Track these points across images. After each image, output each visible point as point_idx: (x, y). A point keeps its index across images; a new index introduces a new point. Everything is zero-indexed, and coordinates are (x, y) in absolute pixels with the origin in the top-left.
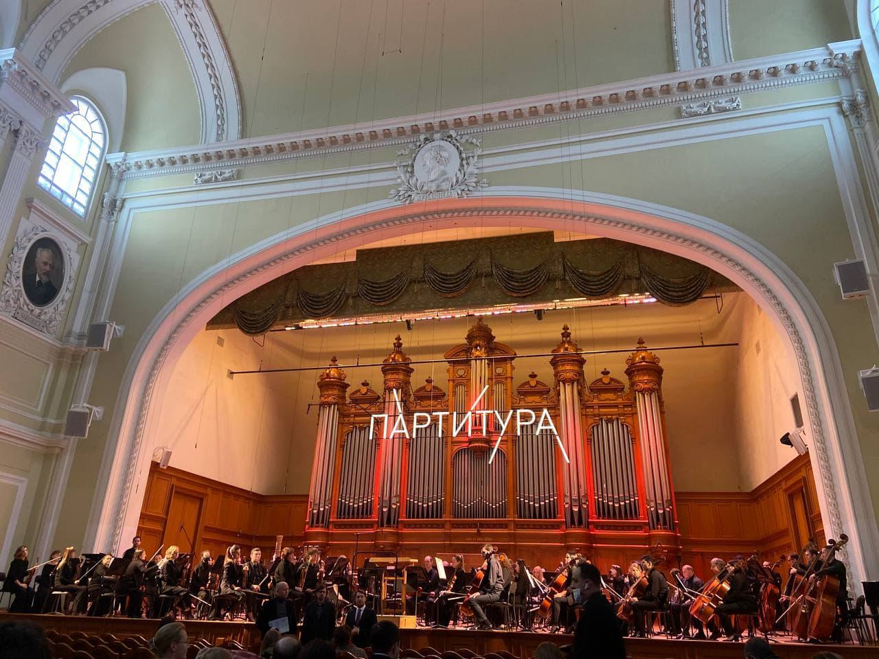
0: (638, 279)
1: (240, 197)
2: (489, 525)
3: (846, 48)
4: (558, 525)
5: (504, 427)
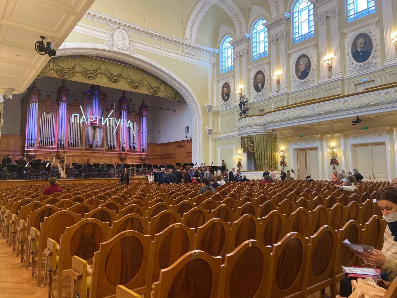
0: (164, 91)
1: (92, 34)
3: (216, 51)
4: (81, 149)
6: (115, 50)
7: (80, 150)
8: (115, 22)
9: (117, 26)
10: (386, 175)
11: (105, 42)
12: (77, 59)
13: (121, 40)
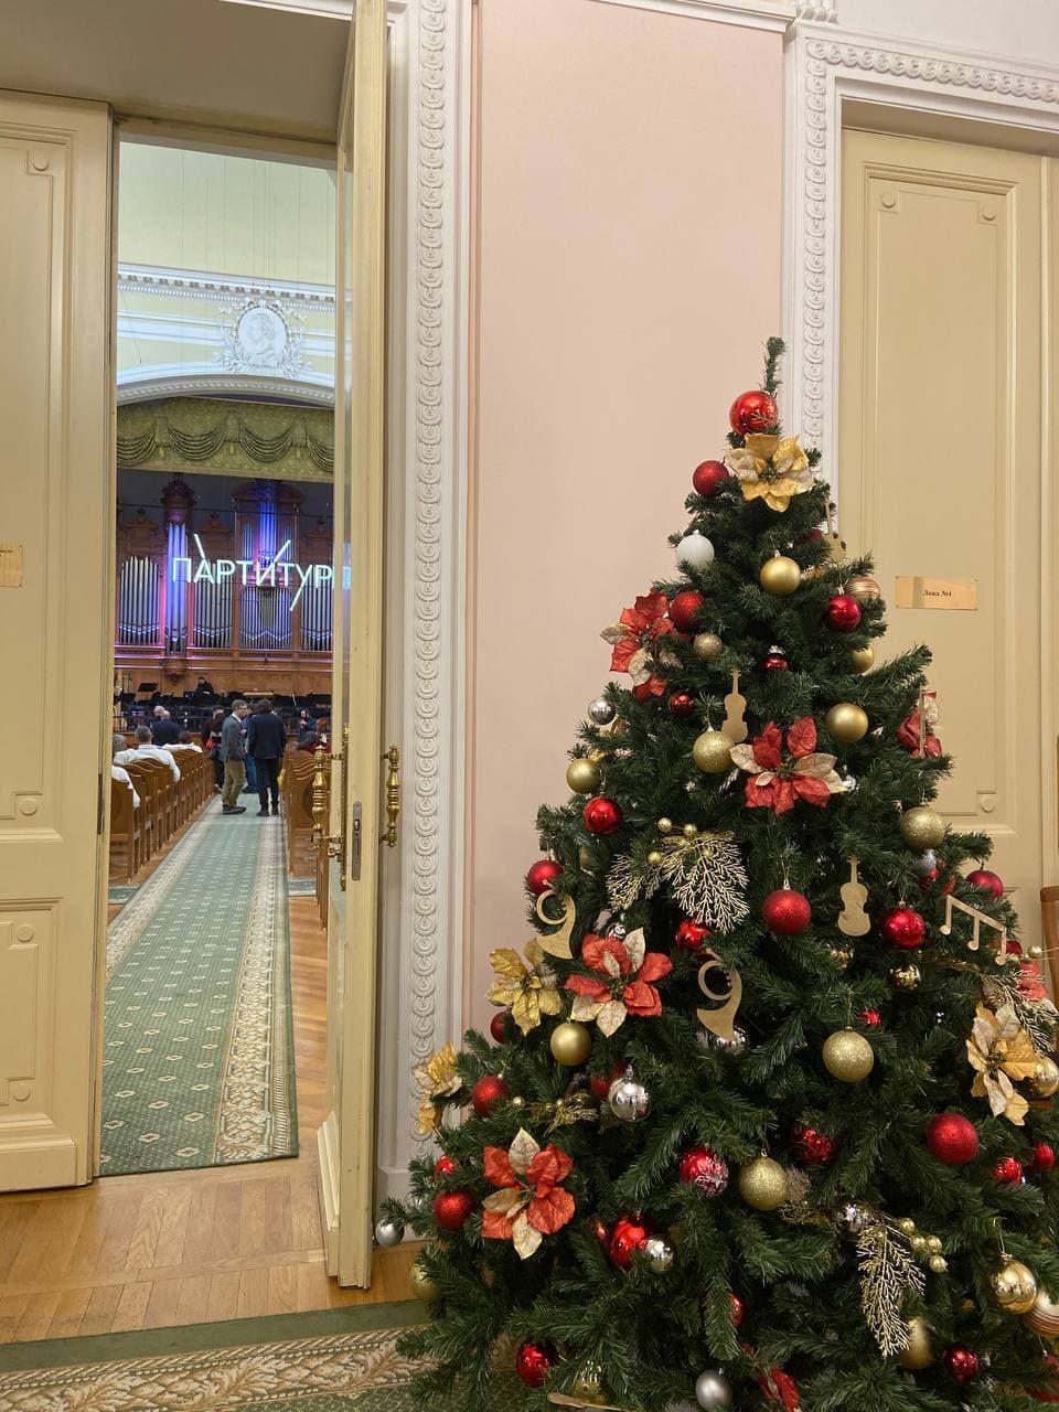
2: (275, 655)
5: (304, 580)
6: (242, 372)
7: (226, 654)
8: (240, 290)
9: (248, 300)
10: (291, 893)
11: (216, 354)
12: (159, 410)
13: (261, 339)
